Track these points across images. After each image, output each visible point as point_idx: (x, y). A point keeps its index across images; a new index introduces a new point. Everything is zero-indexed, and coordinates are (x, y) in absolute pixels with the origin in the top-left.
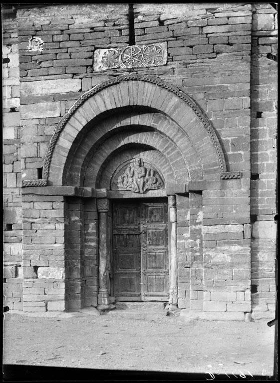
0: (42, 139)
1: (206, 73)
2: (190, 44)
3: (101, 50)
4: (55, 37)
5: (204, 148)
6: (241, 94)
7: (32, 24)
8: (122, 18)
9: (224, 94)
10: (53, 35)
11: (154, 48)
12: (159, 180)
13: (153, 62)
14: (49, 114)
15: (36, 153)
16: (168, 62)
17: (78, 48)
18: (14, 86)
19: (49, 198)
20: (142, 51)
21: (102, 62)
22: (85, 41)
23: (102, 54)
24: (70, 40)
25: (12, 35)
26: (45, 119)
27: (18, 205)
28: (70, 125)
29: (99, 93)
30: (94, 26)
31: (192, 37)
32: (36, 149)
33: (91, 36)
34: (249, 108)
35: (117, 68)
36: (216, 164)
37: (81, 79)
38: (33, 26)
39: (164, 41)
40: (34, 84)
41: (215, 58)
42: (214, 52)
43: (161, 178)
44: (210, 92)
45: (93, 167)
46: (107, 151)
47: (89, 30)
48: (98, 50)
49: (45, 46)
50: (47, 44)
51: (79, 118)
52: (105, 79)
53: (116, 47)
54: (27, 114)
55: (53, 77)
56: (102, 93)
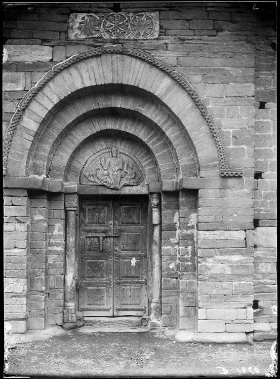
13: (142, 34)
16: (159, 35)
23: (79, 20)
35: (98, 38)
39: (156, 11)
41: (215, 36)
45: (61, 156)
51: (49, 94)
52: (83, 49)
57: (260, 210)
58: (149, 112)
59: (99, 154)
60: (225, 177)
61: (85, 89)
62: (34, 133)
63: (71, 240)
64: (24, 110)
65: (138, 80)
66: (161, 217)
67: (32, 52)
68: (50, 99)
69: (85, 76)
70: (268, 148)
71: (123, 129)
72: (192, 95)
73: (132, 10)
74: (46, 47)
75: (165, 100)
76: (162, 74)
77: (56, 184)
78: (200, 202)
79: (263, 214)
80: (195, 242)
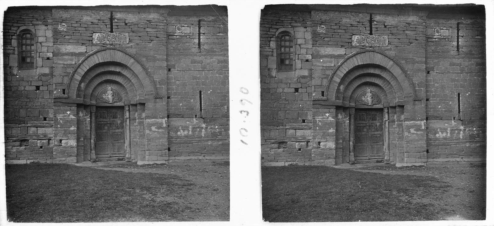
0: (325, 76)
1: (147, 49)
2: (139, 35)
3: (97, 34)
4: (73, 25)
5: (405, 86)
6: (421, 62)
7: (320, 18)
8: (107, 19)
9: (154, 59)
10: (72, 23)
11: (123, 35)
12: (379, 99)
13: (122, 41)
14: (69, 62)
15: (62, 81)
16: (129, 42)
17: (84, 31)
18: (49, 46)
19: (328, 107)
20: (117, 36)
21: (97, 39)
22: (348, 31)
23: (356, 38)
24: (81, 27)
25: (48, 21)
26: (326, 66)
27: (51, 108)
28: (80, 68)
29: (355, 56)
30: (353, 24)
31: (140, 32)
32: (62, 79)
33: (351, 28)
34: (425, 69)
35: (105, 43)
36: (410, 93)
37: (86, 46)
38: (321, 19)
39: (127, 33)
40: (61, 47)
41: (151, 43)
42: (150, 40)
43: (380, 99)
44: (408, 60)
45: (348, 92)
46: (355, 85)
47: (350, 25)
48: (95, 33)
49: (327, 30)
50: (69, 27)
51: (85, 65)
52: (358, 50)
53: (364, 35)
54: (57, 61)
55: (331, 46)
56: (97, 54)
57: (429, 114)
58: (384, 75)
59: (363, 91)
60: (156, 98)
61: (100, 63)
62: (79, 81)
63: (93, 125)
64: (75, 72)
65: (380, 62)
66: (130, 115)
67: (338, 51)
68: (345, 69)
69: (359, 60)
70: (172, 87)
71: (373, 81)
72: (142, 66)
73: (118, 32)
74: (343, 49)
75: (132, 68)
76: (130, 57)
77: (347, 104)
78: (146, 108)
79: (430, 115)
80: (144, 124)
